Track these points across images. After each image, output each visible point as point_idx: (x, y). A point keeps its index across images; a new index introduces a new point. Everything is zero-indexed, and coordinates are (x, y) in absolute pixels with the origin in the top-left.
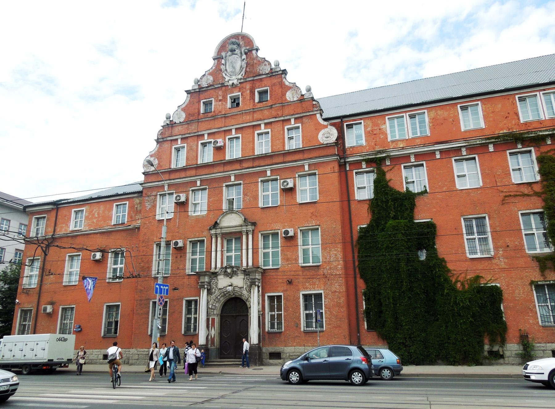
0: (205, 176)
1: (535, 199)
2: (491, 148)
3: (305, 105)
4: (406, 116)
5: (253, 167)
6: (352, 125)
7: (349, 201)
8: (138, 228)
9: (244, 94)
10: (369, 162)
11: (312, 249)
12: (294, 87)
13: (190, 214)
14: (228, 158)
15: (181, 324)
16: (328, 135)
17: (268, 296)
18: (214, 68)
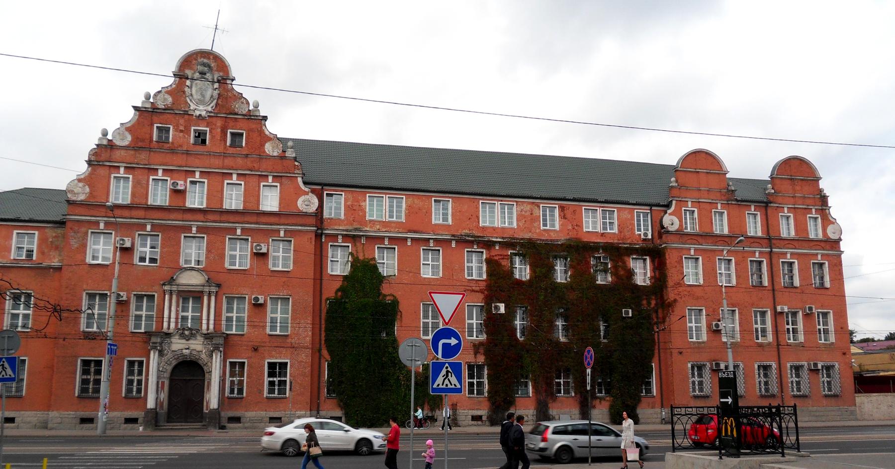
2: (454, 245)
11: (279, 316)
18: (174, 86)
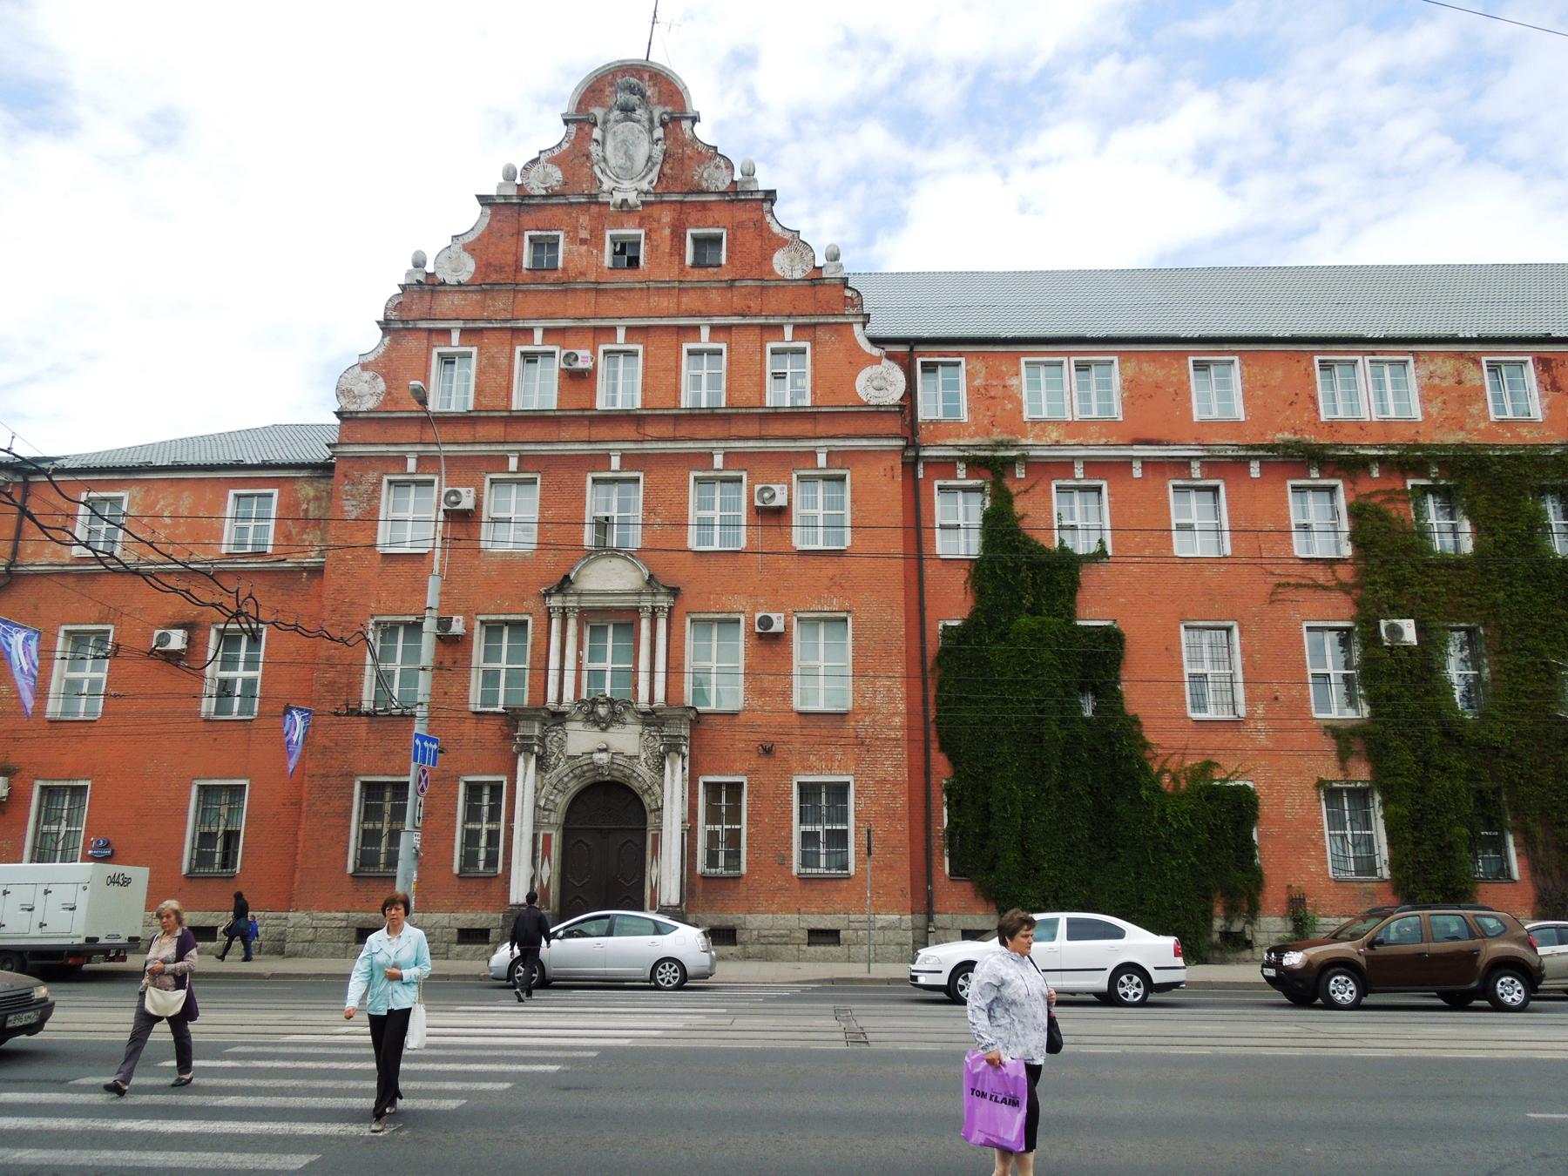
0: (532, 447)
1: (1338, 598)
2: (1255, 470)
3: (822, 294)
4: (1069, 363)
5: (674, 439)
6: (936, 365)
7: (920, 559)
8: (317, 572)
9: (654, 236)
10: (976, 465)
11: (823, 675)
12: (793, 241)
13: (483, 545)
14: (601, 404)
15: (453, 847)
16: (882, 383)
17: (706, 784)
18: (565, 146)
